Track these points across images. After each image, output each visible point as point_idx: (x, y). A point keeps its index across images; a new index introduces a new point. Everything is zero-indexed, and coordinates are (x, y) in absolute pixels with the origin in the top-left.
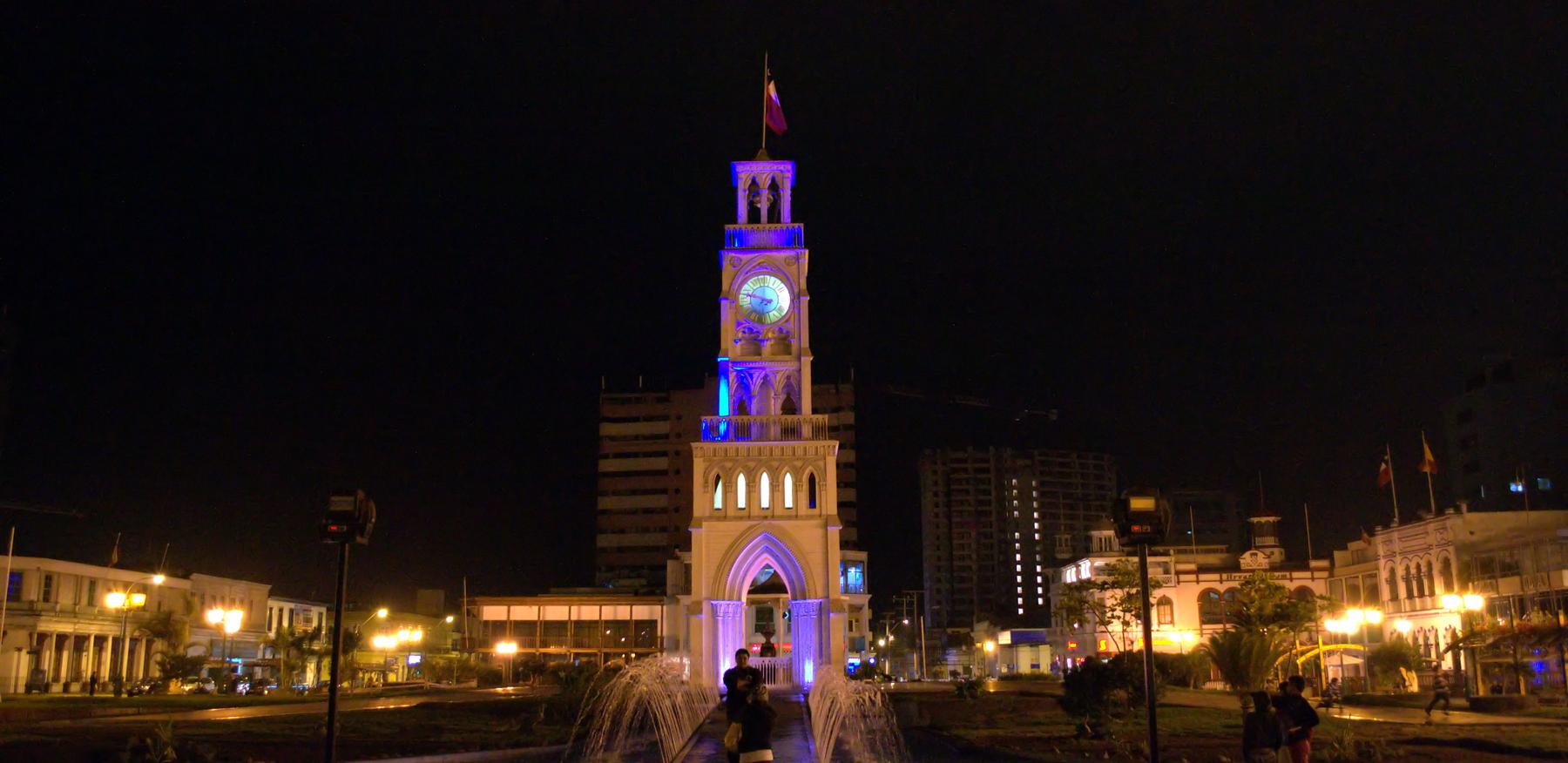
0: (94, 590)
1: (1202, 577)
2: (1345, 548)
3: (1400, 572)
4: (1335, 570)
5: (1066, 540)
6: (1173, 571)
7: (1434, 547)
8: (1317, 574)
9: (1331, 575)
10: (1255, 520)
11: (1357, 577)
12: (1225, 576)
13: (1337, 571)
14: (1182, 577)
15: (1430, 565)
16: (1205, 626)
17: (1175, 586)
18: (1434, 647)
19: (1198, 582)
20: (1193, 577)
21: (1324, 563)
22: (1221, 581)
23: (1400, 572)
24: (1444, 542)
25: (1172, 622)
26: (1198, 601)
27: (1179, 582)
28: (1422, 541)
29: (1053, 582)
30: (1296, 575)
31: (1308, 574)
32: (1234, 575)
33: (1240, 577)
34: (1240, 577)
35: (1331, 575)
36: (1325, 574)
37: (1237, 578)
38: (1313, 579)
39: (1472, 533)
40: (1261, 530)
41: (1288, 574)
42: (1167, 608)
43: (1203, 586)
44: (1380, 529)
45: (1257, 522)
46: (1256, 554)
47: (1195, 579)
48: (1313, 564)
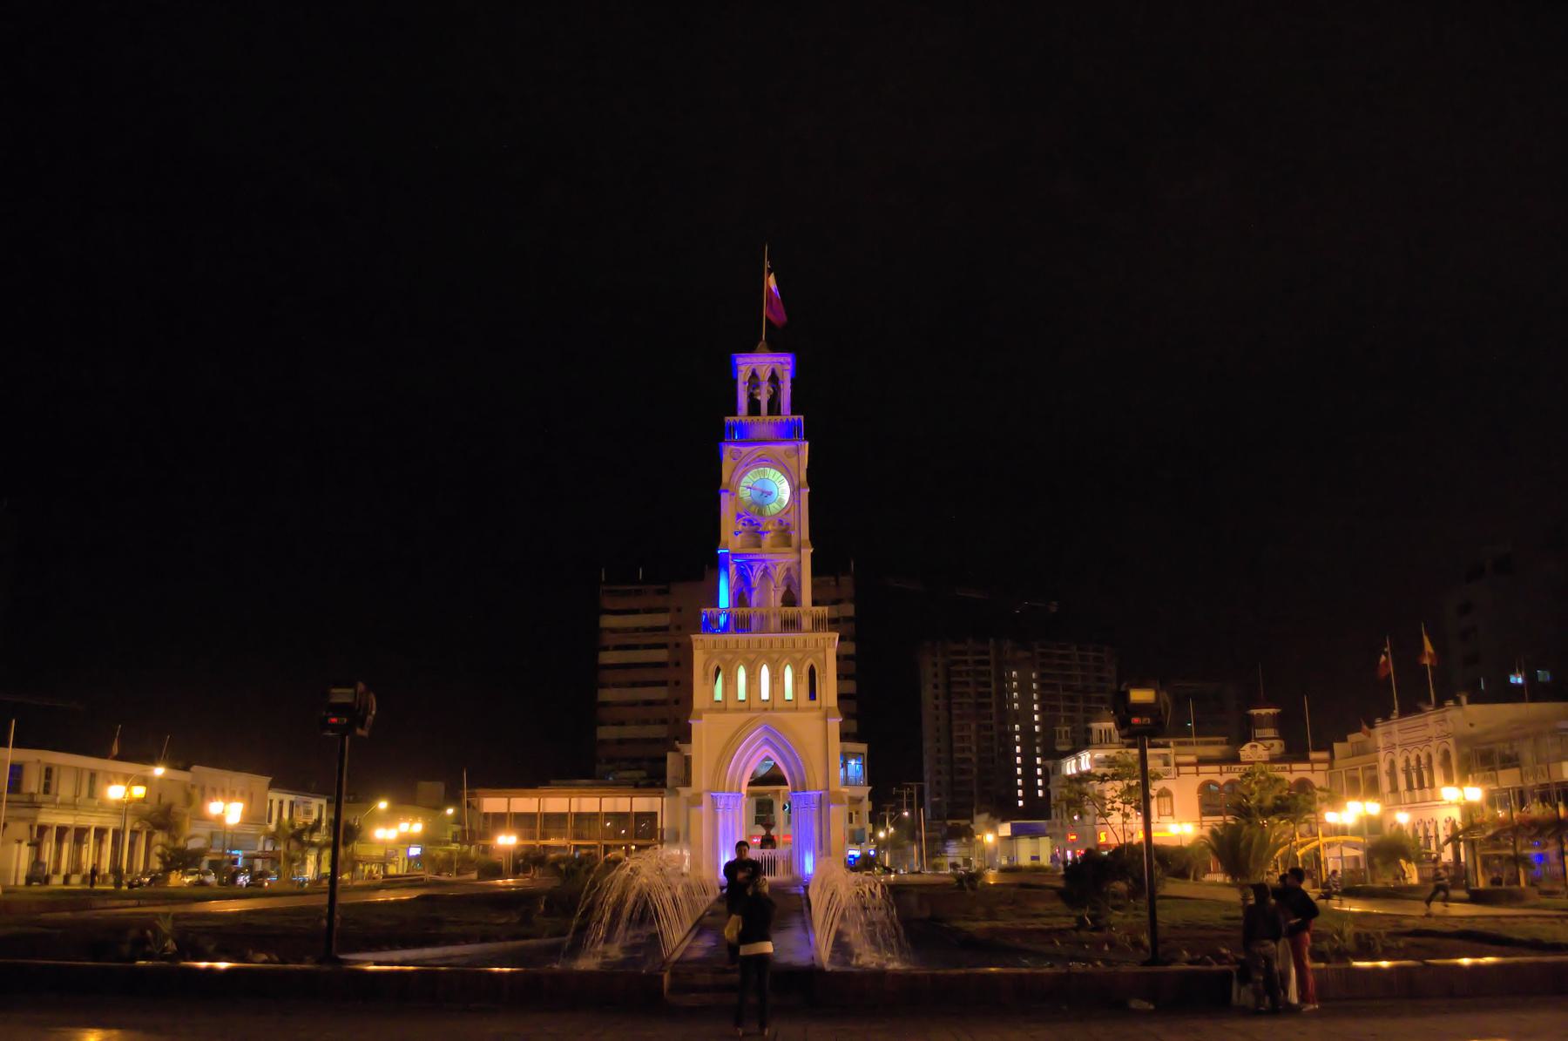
1: (1202, 769)
2: (1344, 740)
3: (1400, 764)
5: (1066, 732)
6: (1173, 763)
8: (1317, 766)
9: (1331, 767)
14: (1182, 769)
15: (1429, 757)
20: (1193, 769)
21: (1325, 755)
23: (1400, 764)
26: (1198, 793)
27: (1178, 774)
30: (1296, 766)
32: (1234, 767)
35: (1331, 767)
36: (1325, 766)
37: (1237, 770)
38: (1313, 771)
39: (1471, 725)
41: (1287, 766)
42: (1167, 799)
43: (1203, 778)
47: (1195, 771)
48: (1313, 755)
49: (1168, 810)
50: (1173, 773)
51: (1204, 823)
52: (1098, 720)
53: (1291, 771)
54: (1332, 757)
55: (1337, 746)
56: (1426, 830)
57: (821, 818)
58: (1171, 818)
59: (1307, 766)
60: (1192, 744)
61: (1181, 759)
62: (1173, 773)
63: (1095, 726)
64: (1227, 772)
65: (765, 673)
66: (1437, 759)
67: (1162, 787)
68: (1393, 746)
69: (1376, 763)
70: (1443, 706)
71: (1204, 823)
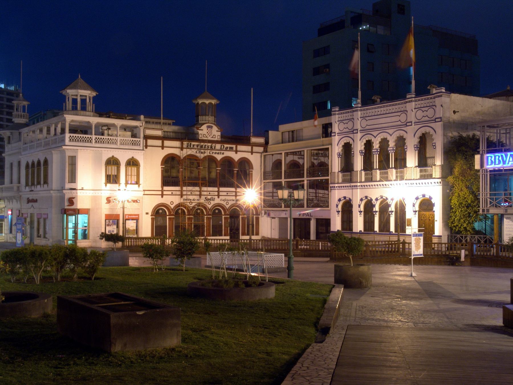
0: (439, 263)
1: (167, 143)
2: (277, 129)
3: (359, 147)
4: (269, 146)
5: (24, 107)
6: (142, 135)
7: (18, 185)
8: (256, 149)
9: (265, 151)
10: (200, 101)
11: (281, 154)
12: (185, 143)
13: (270, 147)
14: (150, 142)
15: (401, 142)
16: (165, 188)
17: (143, 150)
18: (394, 213)
19: (163, 147)
20: (159, 143)
21: (262, 140)
22: (182, 148)
23: (359, 147)
24: (347, 130)
25: (137, 183)
26: (162, 165)
27: (146, 146)
28: (397, 119)
29: (9, 143)
30: (240, 148)
31: (248, 148)
32: (193, 143)
33: (197, 146)
34: (197, 146)
35: (265, 151)
36: (261, 149)
37: (195, 147)
38: (252, 153)
39: (454, 112)
40: (205, 110)
41: (234, 146)
42: (134, 169)
43: (168, 151)
44: (337, 109)
45: (202, 103)
46: (211, 127)
47: (161, 145)
48: (254, 140)
49: (134, 179)
50: (141, 145)
51: (203, 193)
52: (75, 87)
53: (236, 152)
54: (267, 143)
55: (271, 133)
56: (167, 181)
57: (46, 149)
58: (137, 186)
59: (248, 148)
60: (160, 123)
61: (149, 132)
62: (141, 145)
63: (70, 92)
64: (187, 148)
65: (130, 244)
66: (411, 143)
67: (111, 156)
68: (354, 131)
69: (330, 147)
70: (427, 92)
71: (203, 193)
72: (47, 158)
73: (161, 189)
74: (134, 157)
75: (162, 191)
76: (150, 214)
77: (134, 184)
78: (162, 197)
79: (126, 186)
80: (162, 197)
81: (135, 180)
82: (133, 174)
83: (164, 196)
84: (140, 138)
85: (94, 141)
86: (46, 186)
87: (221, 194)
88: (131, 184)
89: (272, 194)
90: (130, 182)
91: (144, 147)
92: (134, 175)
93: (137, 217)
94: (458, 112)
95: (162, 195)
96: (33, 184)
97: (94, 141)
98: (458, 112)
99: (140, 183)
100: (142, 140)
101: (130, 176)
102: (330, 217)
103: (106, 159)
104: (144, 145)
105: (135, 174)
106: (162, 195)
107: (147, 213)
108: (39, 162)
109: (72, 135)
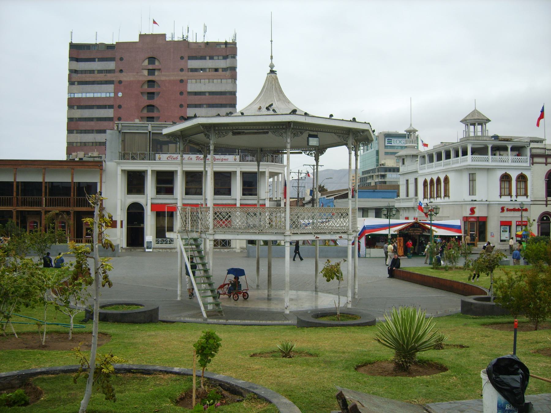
14: (536, 160)
72: (439, 176)
73: (545, 199)
74: (523, 173)
75: (546, 201)
76: (536, 220)
77: (507, 195)
78: (546, 206)
79: (517, 197)
80: (546, 206)
81: (524, 193)
82: (506, 187)
83: (548, 205)
84: (526, 156)
85: (490, 160)
86: (446, 199)
87: (267, 193)
88: (505, 195)
89: (548, 199)
90: (519, 194)
91: (531, 164)
92: (507, 188)
93: (526, 223)
94: (97, 32)
95: (546, 205)
96: (431, 197)
97: (490, 160)
98: (97, 32)
99: (528, 195)
100: (529, 158)
101: (503, 189)
102: (370, 217)
103: (527, 176)
104: (531, 162)
105: (508, 187)
106: (546, 205)
107: (534, 220)
108: (438, 180)
109: (473, 156)
